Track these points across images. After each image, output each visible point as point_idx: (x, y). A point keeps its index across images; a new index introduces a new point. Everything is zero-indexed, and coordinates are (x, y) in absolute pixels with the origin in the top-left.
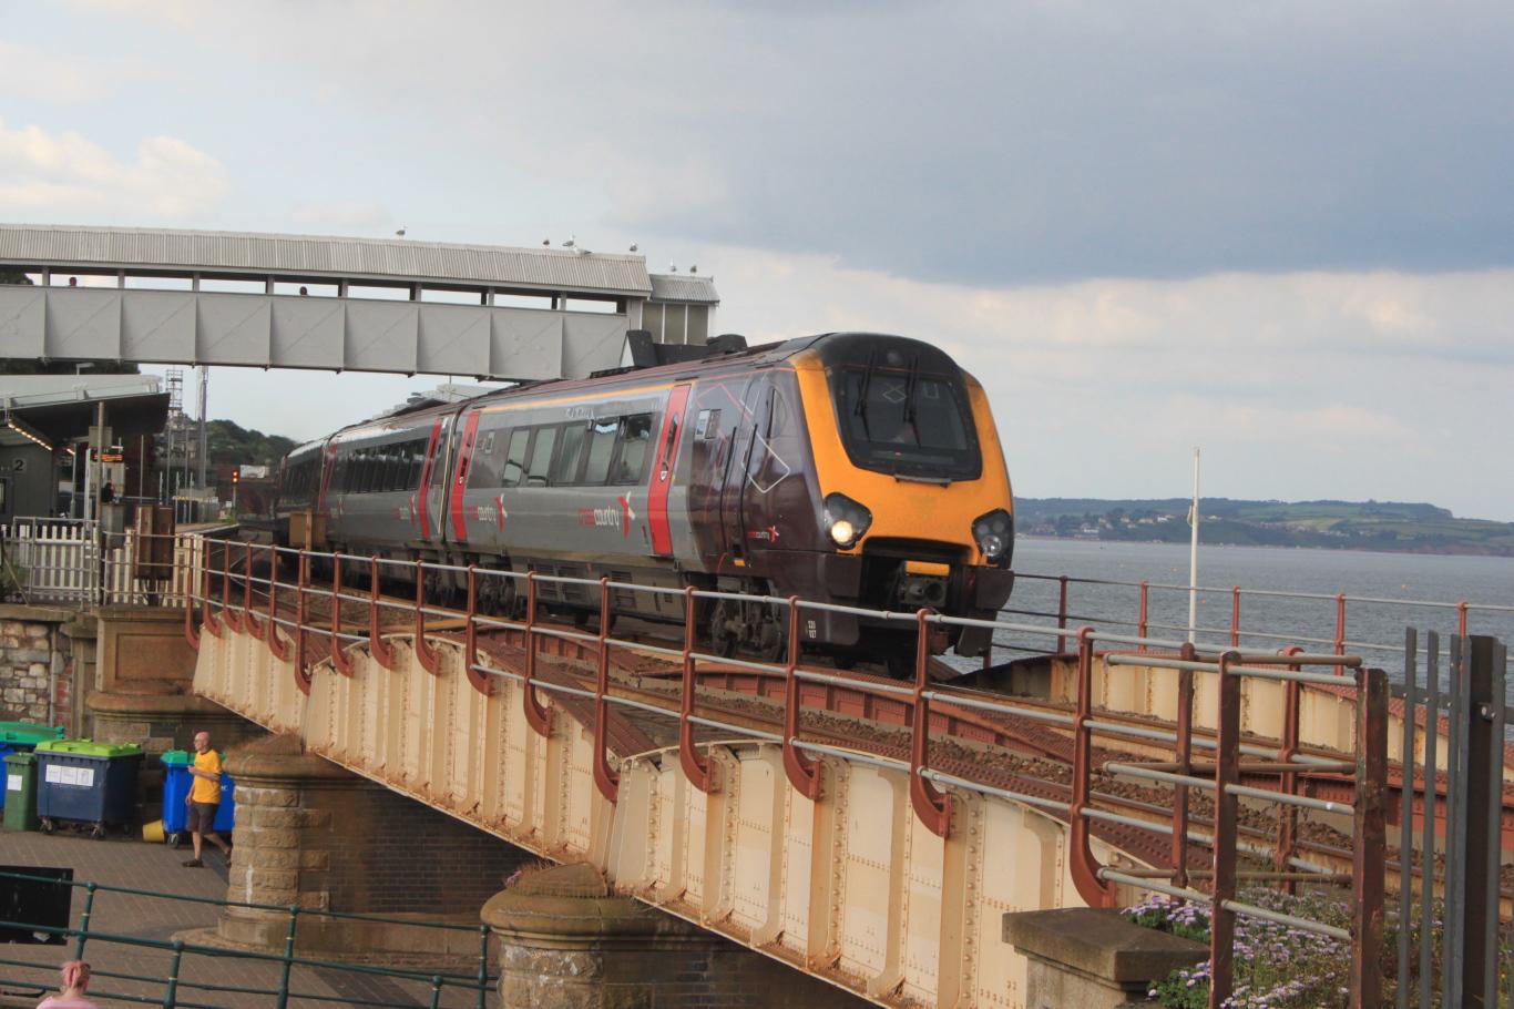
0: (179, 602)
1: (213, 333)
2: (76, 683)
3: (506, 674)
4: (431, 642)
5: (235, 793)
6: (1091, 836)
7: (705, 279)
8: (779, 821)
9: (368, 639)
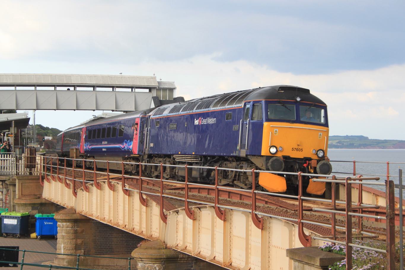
0: (37, 174)
1: (81, 101)
2: (10, 196)
3: (133, 190)
4: (111, 182)
5: (58, 224)
6: (304, 228)
7: (172, 82)
8: (213, 226)
9: (93, 182)
